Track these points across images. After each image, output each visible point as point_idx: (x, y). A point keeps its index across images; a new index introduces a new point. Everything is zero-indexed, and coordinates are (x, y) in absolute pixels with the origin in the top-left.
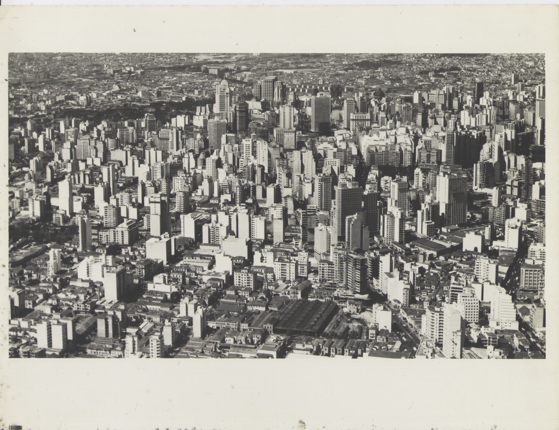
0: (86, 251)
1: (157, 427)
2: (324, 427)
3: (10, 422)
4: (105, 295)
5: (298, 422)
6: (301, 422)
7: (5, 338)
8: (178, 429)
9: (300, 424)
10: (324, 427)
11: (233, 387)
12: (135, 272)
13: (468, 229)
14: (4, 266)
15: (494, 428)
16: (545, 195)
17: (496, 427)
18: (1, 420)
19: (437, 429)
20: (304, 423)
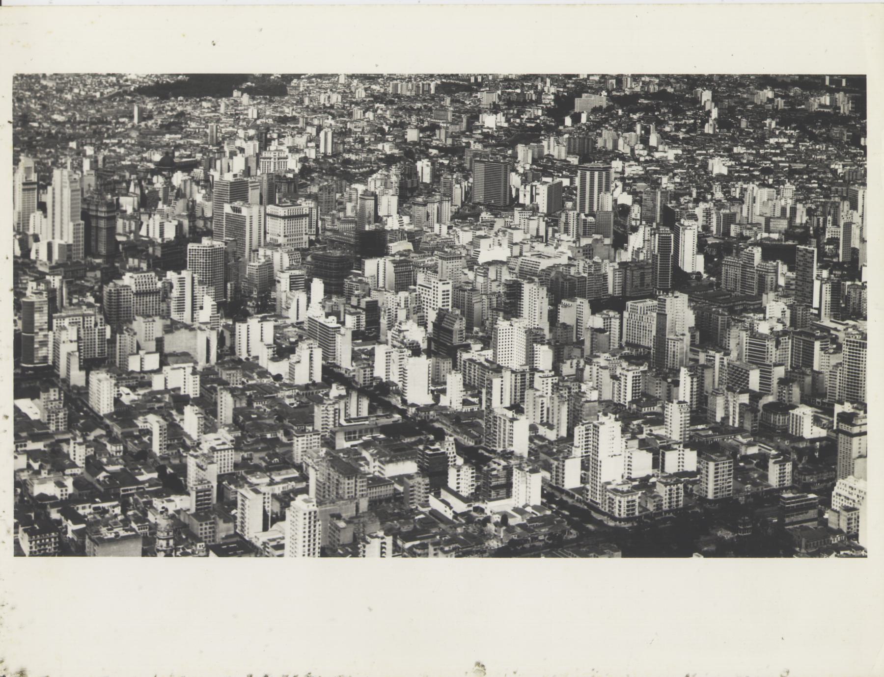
0: (741, 461)
1: (249, 673)
2: (515, 673)
3: (13, 667)
4: (399, 559)
5: (474, 664)
6: (478, 664)
7: (9, 532)
8: (283, 676)
9: (477, 667)
10: (515, 673)
11: (370, 609)
12: (368, 464)
13: (754, 366)
14: (7, 417)
15: (785, 674)
16: (15, 374)
17: (788, 672)
18: (2, 662)
19: (694, 676)
20: (483, 666)
